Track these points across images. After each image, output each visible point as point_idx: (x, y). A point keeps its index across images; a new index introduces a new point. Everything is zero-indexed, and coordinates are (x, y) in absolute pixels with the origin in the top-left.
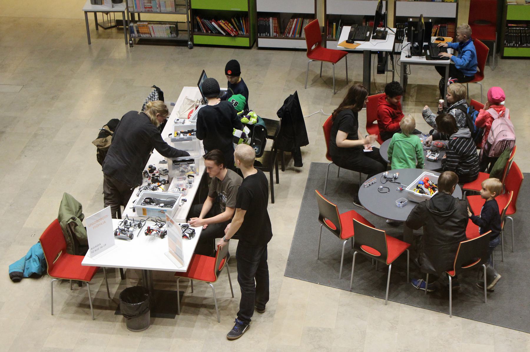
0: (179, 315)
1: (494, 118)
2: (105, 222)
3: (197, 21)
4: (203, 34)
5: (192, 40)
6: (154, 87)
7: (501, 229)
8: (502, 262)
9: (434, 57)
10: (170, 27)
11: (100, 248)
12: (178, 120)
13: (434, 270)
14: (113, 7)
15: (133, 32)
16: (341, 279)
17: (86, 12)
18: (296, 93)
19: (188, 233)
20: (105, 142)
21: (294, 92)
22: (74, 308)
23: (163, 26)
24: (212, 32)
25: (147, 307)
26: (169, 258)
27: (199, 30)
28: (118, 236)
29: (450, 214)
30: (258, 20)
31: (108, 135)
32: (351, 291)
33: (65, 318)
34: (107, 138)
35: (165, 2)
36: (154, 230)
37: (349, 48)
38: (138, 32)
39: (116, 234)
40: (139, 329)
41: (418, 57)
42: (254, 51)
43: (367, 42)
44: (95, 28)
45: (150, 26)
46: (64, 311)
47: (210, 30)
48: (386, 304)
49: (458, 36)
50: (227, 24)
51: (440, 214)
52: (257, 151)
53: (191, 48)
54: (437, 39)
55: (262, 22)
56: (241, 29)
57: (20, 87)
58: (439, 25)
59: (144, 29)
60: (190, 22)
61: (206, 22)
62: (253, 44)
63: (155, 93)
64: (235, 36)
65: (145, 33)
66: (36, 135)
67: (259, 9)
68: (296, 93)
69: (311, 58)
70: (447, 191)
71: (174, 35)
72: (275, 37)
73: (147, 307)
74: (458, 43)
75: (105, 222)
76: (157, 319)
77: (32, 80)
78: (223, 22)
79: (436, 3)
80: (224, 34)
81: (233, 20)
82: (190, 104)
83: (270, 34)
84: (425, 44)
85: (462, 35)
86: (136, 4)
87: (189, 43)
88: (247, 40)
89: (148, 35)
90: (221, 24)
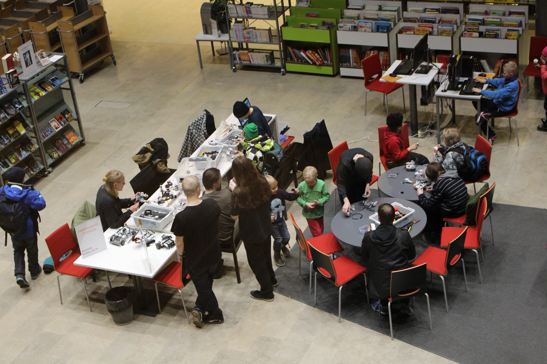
0: (160, 314)
2: (95, 229)
3: (289, 52)
4: (294, 62)
5: (284, 67)
6: (206, 111)
8: (465, 292)
9: (467, 92)
10: (266, 56)
11: (91, 251)
12: (212, 141)
13: (378, 296)
14: (219, 36)
16: (311, 295)
17: (198, 41)
18: (323, 122)
19: (168, 244)
20: (142, 158)
21: (321, 120)
22: (81, 300)
23: (261, 54)
24: (301, 61)
25: (126, 306)
28: (112, 242)
29: (391, 243)
30: (339, 51)
31: (147, 152)
32: (314, 307)
33: (70, 308)
34: (145, 155)
35: (261, 34)
36: (140, 239)
38: (240, 59)
39: (111, 240)
40: (121, 323)
41: (453, 91)
42: (337, 78)
44: (212, 54)
46: (73, 302)
47: (301, 60)
48: (340, 322)
49: (505, 74)
50: (313, 54)
51: (381, 243)
52: (267, 173)
53: (283, 74)
54: (480, 75)
58: (502, 60)
59: (245, 57)
61: (296, 51)
62: (336, 74)
63: (204, 116)
64: (320, 65)
65: (245, 60)
66: (122, 147)
67: (339, 42)
68: (323, 122)
69: (368, 88)
72: (355, 67)
73: (126, 306)
74: (504, 79)
75: (95, 229)
76: (141, 316)
78: (310, 52)
79: (509, 40)
80: (311, 63)
81: (319, 51)
82: (225, 128)
83: (350, 64)
84: (462, 79)
85: (509, 73)
86: (236, 35)
87: (282, 70)
88: (331, 68)
89: (248, 62)
90: (308, 54)
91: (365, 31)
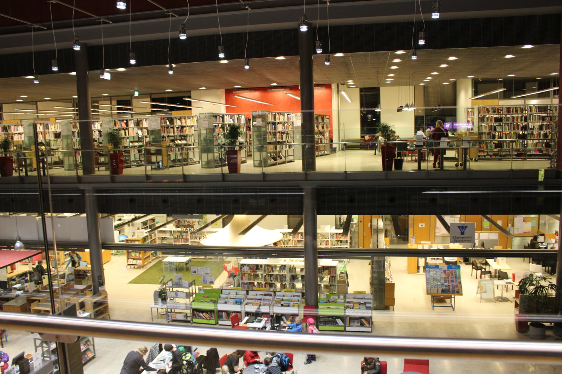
5: (192, 321)
7: (394, 154)
15: (169, 317)
17: (151, 308)
26: (357, 299)
27: (196, 316)
38: (171, 317)
43: (252, 324)
45: (176, 314)
55: (220, 314)
56: (212, 317)
61: (198, 313)
64: (209, 320)
70: (438, 164)
71: (185, 318)
72: (225, 320)
88: (214, 321)
91: (230, 304)
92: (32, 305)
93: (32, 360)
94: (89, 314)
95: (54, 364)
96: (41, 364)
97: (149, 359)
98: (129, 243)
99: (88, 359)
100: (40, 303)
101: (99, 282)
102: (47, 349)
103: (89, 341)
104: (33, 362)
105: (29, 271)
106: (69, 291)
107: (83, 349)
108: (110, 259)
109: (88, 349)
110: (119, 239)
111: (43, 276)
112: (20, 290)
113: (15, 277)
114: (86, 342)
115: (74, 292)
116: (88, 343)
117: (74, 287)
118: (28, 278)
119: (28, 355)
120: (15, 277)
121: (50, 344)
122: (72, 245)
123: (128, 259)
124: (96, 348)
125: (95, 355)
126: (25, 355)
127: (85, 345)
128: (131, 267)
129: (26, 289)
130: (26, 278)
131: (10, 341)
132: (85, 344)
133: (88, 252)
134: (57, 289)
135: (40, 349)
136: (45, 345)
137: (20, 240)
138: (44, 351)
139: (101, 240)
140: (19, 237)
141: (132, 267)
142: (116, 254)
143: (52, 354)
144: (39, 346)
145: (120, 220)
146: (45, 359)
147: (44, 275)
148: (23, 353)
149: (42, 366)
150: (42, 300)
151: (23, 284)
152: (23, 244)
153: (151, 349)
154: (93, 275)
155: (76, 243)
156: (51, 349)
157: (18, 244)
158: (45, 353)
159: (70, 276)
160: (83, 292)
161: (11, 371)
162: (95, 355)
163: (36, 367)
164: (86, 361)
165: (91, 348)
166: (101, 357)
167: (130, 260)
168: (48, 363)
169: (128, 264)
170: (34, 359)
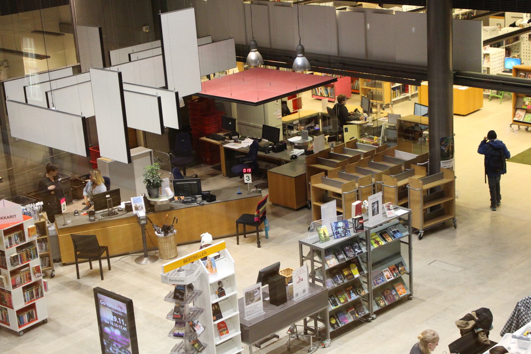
1: (206, 76)
34: (469, 322)
37: (411, 204)
57: (460, 269)
60: (145, 229)
77: (474, 266)
92: (313, 178)
93: (291, 281)
94: (407, 212)
95: (330, 297)
96: (307, 291)
97: (511, 325)
98: (521, 77)
99: (397, 298)
100: (327, 178)
101: (442, 151)
102: (320, 265)
103: (401, 264)
104: (292, 285)
105: (322, 114)
106: (384, 161)
107: (388, 278)
108: (481, 106)
109: (398, 280)
110: (504, 65)
111: (345, 126)
112: (299, 147)
113: (298, 121)
114: (397, 266)
115: (392, 165)
116: (400, 268)
117: (394, 156)
118: (320, 126)
119: (288, 270)
120: (298, 121)
121: (326, 258)
122: (398, 71)
123: (516, 109)
124: (414, 280)
125: (411, 295)
126: (281, 269)
127: (392, 270)
128: (521, 127)
129: (309, 149)
130: (317, 127)
131: (273, 239)
132: (394, 269)
133: (425, 86)
134: (362, 155)
135: (308, 262)
136: (316, 258)
137: (304, 53)
138: (315, 268)
139: (27, 42)
140: (302, 46)
141: (523, 127)
142: (493, 98)
143: (328, 277)
144: (307, 258)
145: (513, 25)
146: (317, 283)
147: (347, 124)
148: (278, 265)
149: (307, 294)
150: (331, 171)
151: (305, 137)
152: (309, 60)
153: (517, 306)
154: (431, 136)
155: (406, 67)
156: (327, 268)
157: (299, 61)
158: (317, 272)
159: (390, 131)
160: (410, 168)
161: (255, 292)
162: (411, 295)
163: (297, 295)
164: (393, 301)
165: (405, 278)
166: (423, 300)
167: (519, 112)
168: (318, 291)
169: (515, 121)
170: (295, 280)
